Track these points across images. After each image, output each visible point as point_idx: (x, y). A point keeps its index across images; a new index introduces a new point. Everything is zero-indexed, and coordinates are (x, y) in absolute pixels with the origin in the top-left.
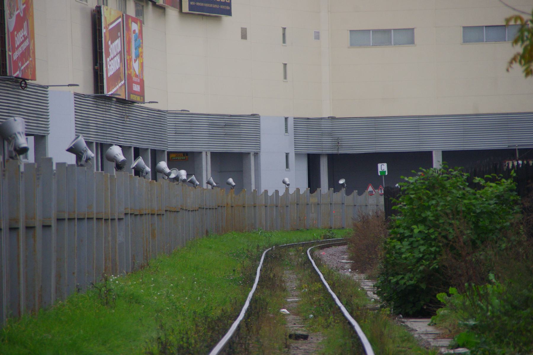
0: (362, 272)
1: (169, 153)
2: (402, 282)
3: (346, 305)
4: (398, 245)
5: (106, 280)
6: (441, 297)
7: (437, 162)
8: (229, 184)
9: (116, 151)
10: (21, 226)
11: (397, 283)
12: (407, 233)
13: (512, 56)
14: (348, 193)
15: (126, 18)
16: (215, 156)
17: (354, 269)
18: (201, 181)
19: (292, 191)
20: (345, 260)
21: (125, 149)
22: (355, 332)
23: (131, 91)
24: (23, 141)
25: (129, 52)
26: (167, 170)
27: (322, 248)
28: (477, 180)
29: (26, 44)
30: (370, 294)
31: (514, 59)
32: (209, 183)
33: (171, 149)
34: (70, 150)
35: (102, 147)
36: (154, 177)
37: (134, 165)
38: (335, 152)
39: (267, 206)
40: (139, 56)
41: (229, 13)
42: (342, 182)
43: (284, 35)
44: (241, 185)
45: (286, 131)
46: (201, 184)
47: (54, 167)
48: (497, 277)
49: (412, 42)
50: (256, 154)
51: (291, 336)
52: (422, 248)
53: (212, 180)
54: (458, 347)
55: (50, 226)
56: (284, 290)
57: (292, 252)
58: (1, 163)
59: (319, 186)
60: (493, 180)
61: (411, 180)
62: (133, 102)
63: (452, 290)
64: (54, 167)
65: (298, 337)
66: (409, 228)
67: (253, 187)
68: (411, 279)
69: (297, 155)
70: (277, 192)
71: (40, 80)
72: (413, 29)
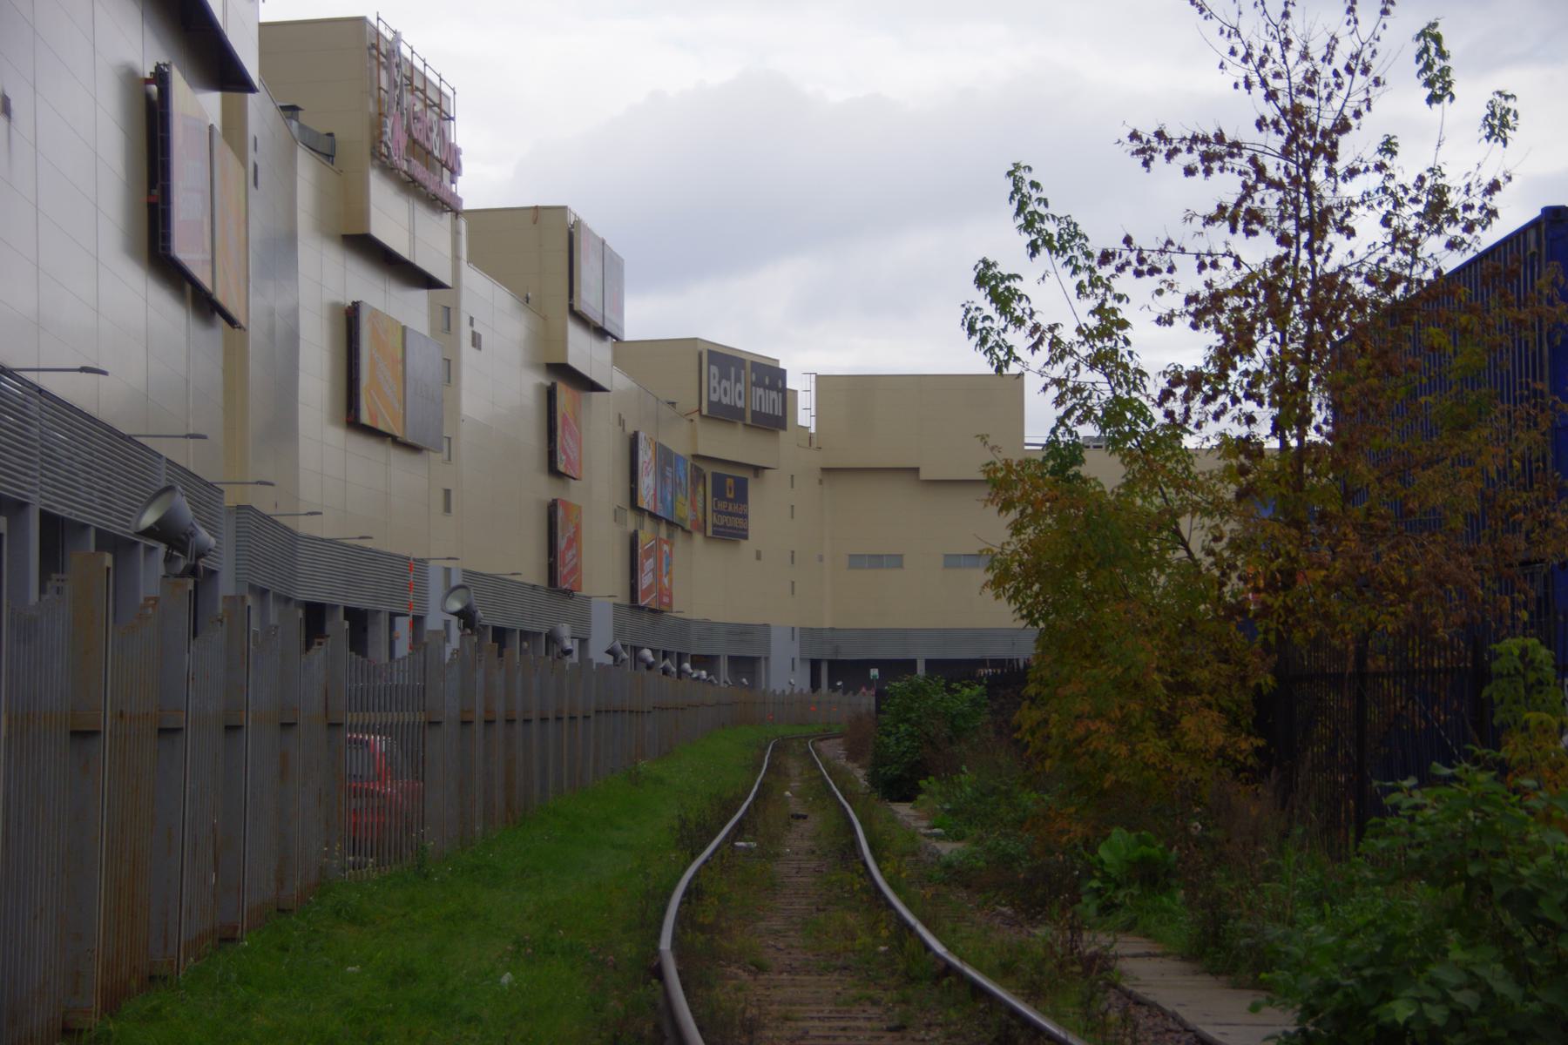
0: (855, 762)
1: (692, 656)
2: (889, 773)
3: (841, 791)
4: (886, 740)
5: (636, 763)
6: (923, 783)
7: (921, 669)
8: (743, 683)
9: (647, 653)
10: (566, 716)
11: (885, 773)
12: (894, 731)
13: (984, 582)
14: (845, 693)
15: (659, 541)
16: (731, 658)
17: (848, 758)
18: (718, 680)
19: (796, 690)
20: (841, 751)
21: (654, 652)
22: (848, 814)
23: (661, 603)
24: (568, 644)
25: (661, 570)
26: (691, 671)
27: (821, 740)
28: (954, 685)
29: (575, 560)
30: (861, 780)
31: (986, 585)
32: (725, 682)
33: (693, 653)
34: (609, 652)
35: (636, 650)
36: (679, 677)
37: (662, 665)
38: (834, 658)
39: (239, 727)
40: (669, 573)
41: (746, 537)
42: (839, 684)
43: (793, 556)
44: (753, 684)
45: (793, 639)
46: (718, 684)
47: (594, 667)
48: (969, 769)
49: (901, 566)
50: (767, 659)
51: (792, 816)
52: (907, 743)
53: (728, 680)
54: (934, 827)
55: (589, 717)
56: (788, 776)
57: (795, 744)
58: (190, 591)
59: (820, 687)
60: (968, 686)
61: (897, 684)
62: (663, 611)
63: (931, 779)
64: (594, 667)
65: (798, 817)
66: (895, 726)
67: (763, 687)
68: (897, 770)
69: (802, 660)
70: (784, 691)
71: (584, 592)
72: (901, 556)
